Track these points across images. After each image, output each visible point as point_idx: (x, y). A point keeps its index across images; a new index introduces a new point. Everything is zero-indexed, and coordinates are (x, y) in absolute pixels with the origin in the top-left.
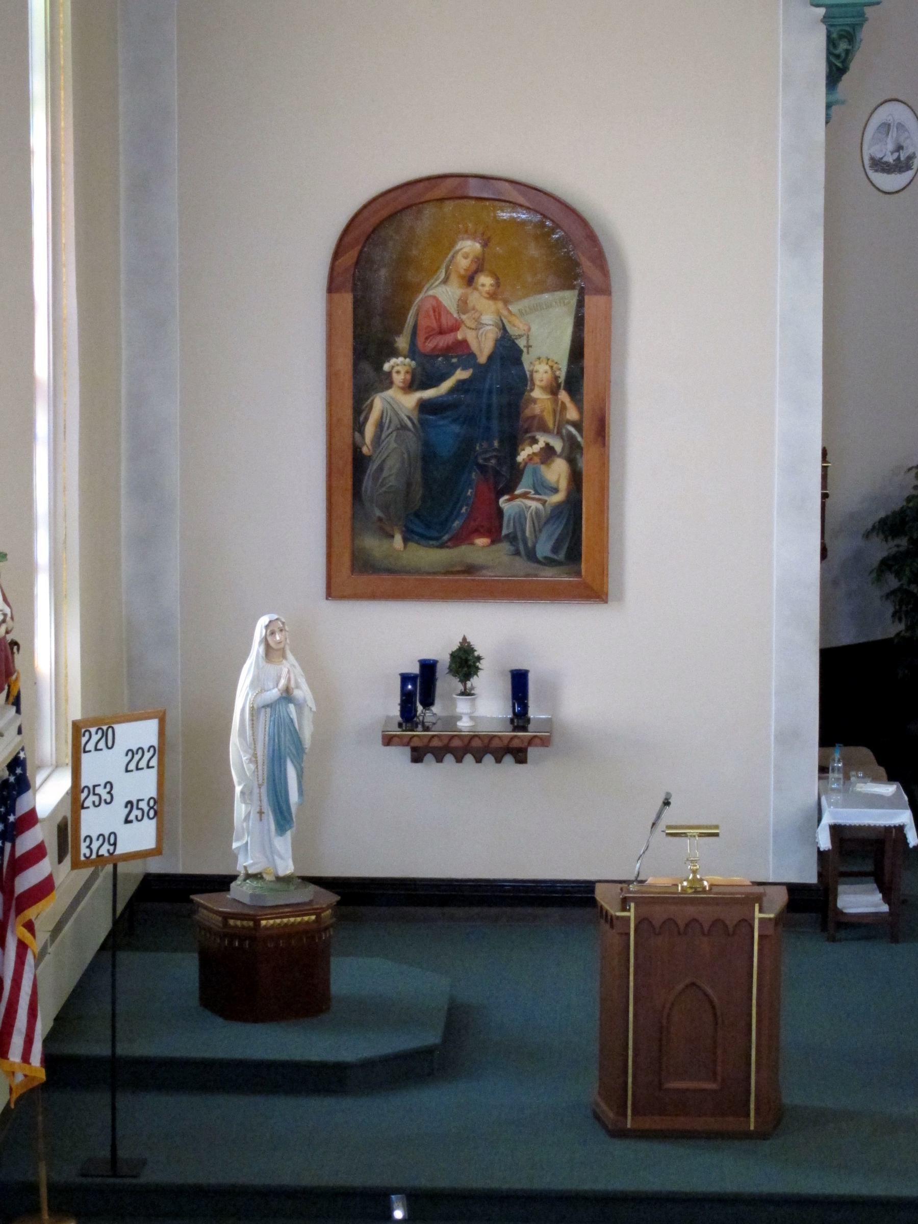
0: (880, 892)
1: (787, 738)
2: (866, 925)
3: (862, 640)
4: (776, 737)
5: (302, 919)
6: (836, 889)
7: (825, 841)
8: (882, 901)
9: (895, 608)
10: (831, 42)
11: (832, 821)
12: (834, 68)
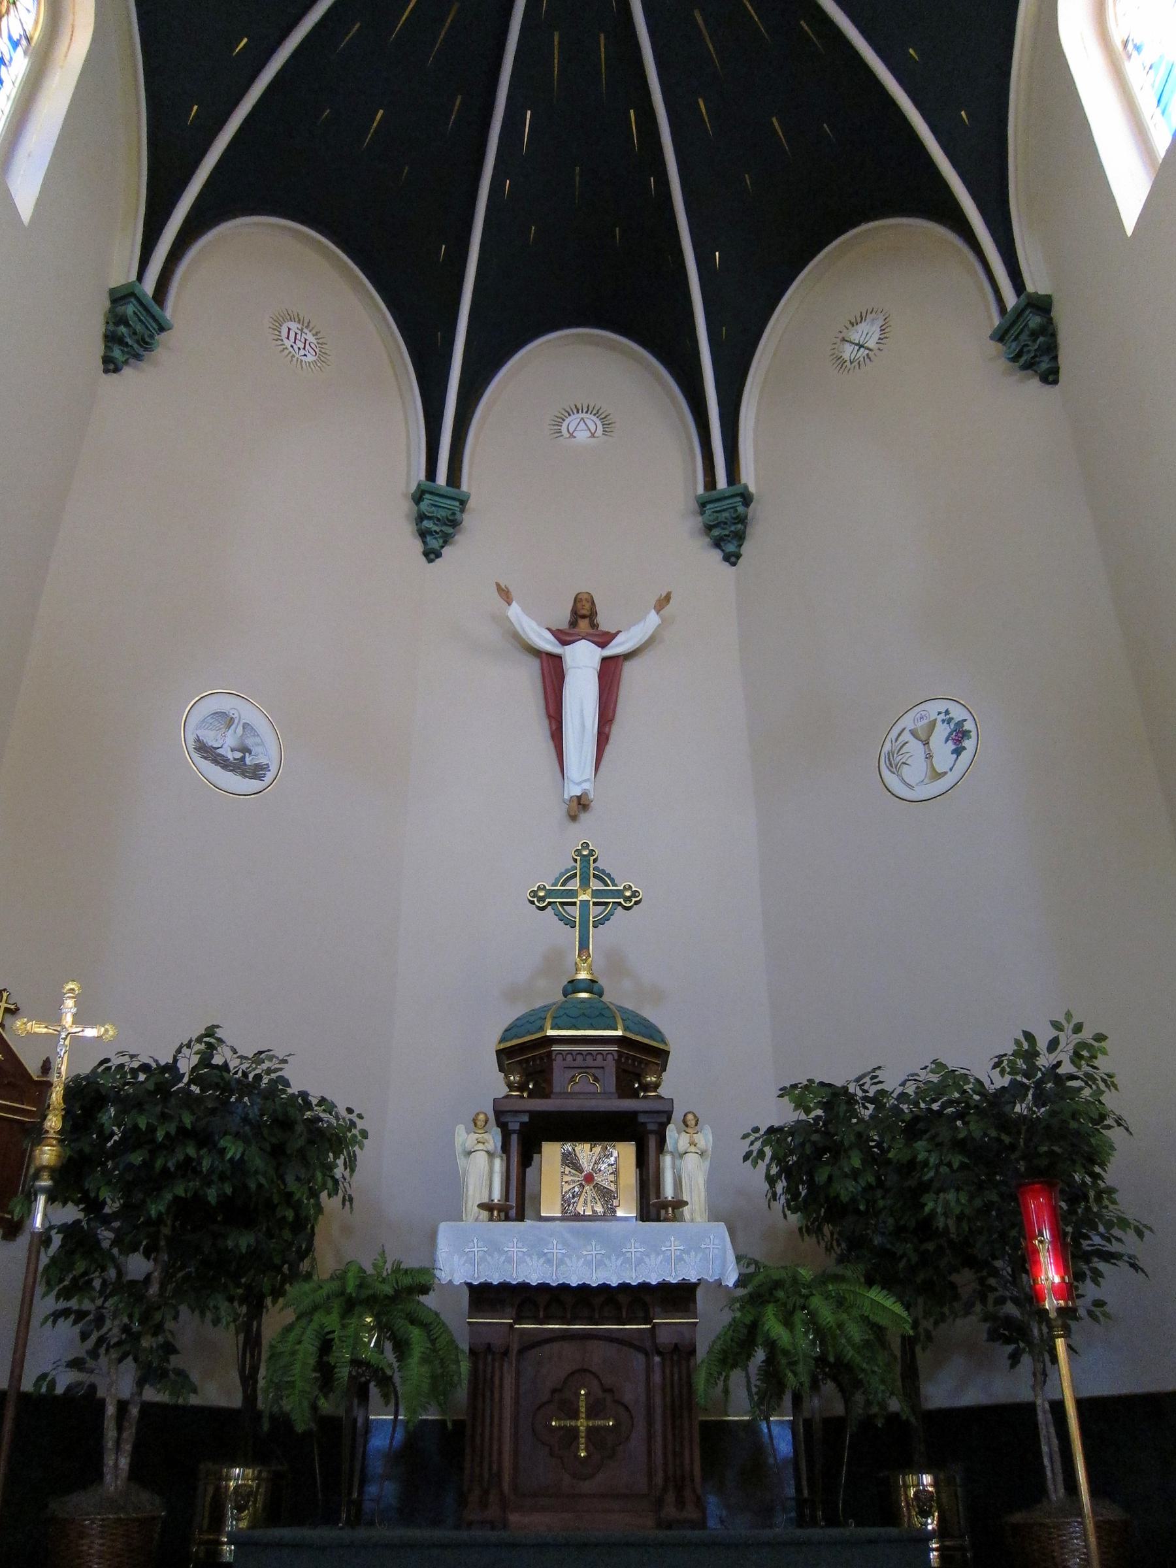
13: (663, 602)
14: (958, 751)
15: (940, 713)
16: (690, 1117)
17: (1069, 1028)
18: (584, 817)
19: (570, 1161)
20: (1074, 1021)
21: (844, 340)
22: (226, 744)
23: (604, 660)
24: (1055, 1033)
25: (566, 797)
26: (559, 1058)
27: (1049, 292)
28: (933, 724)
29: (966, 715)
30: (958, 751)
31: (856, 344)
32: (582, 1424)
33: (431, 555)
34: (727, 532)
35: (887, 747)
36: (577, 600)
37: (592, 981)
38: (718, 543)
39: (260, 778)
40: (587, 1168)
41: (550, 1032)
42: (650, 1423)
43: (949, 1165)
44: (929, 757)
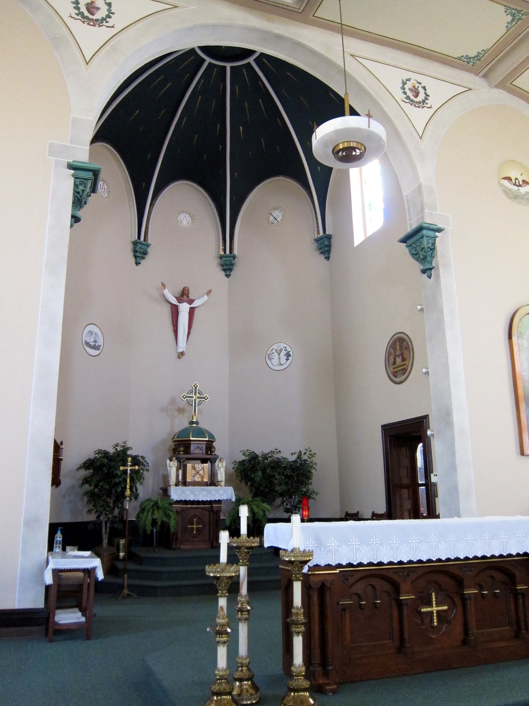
0: (80, 612)
1: (30, 523)
2: (72, 630)
3: (73, 521)
4: (24, 523)
5: (435, 616)
6: (54, 613)
7: (49, 579)
8: (82, 616)
9: (88, 499)
10: (76, 186)
11: (54, 567)
12: (77, 199)
13: (209, 292)
14: (287, 359)
15: (284, 347)
16: (222, 459)
17: (309, 451)
18: (183, 357)
19: (194, 468)
20: (310, 449)
21: (270, 214)
22: (91, 340)
23: (190, 308)
24: (306, 451)
25: (178, 351)
26: (192, 444)
27: (331, 234)
28: (282, 350)
29: (290, 350)
30: (287, 359)
31: (275, 218)
32: (195, 526)
33: (137, 263)
34: (227, 268)
35: (269, 352)
36: (184, 289)
37: (197, 421)
38: (225, 270)
39: (99, 349)
40: (197, 470)
41: (191, 439)
42: (210, 525)
43: (282, 479)
44: (279, 359)
